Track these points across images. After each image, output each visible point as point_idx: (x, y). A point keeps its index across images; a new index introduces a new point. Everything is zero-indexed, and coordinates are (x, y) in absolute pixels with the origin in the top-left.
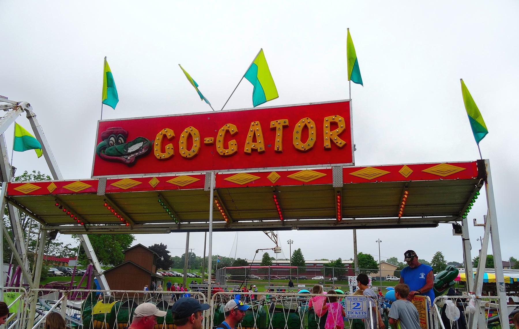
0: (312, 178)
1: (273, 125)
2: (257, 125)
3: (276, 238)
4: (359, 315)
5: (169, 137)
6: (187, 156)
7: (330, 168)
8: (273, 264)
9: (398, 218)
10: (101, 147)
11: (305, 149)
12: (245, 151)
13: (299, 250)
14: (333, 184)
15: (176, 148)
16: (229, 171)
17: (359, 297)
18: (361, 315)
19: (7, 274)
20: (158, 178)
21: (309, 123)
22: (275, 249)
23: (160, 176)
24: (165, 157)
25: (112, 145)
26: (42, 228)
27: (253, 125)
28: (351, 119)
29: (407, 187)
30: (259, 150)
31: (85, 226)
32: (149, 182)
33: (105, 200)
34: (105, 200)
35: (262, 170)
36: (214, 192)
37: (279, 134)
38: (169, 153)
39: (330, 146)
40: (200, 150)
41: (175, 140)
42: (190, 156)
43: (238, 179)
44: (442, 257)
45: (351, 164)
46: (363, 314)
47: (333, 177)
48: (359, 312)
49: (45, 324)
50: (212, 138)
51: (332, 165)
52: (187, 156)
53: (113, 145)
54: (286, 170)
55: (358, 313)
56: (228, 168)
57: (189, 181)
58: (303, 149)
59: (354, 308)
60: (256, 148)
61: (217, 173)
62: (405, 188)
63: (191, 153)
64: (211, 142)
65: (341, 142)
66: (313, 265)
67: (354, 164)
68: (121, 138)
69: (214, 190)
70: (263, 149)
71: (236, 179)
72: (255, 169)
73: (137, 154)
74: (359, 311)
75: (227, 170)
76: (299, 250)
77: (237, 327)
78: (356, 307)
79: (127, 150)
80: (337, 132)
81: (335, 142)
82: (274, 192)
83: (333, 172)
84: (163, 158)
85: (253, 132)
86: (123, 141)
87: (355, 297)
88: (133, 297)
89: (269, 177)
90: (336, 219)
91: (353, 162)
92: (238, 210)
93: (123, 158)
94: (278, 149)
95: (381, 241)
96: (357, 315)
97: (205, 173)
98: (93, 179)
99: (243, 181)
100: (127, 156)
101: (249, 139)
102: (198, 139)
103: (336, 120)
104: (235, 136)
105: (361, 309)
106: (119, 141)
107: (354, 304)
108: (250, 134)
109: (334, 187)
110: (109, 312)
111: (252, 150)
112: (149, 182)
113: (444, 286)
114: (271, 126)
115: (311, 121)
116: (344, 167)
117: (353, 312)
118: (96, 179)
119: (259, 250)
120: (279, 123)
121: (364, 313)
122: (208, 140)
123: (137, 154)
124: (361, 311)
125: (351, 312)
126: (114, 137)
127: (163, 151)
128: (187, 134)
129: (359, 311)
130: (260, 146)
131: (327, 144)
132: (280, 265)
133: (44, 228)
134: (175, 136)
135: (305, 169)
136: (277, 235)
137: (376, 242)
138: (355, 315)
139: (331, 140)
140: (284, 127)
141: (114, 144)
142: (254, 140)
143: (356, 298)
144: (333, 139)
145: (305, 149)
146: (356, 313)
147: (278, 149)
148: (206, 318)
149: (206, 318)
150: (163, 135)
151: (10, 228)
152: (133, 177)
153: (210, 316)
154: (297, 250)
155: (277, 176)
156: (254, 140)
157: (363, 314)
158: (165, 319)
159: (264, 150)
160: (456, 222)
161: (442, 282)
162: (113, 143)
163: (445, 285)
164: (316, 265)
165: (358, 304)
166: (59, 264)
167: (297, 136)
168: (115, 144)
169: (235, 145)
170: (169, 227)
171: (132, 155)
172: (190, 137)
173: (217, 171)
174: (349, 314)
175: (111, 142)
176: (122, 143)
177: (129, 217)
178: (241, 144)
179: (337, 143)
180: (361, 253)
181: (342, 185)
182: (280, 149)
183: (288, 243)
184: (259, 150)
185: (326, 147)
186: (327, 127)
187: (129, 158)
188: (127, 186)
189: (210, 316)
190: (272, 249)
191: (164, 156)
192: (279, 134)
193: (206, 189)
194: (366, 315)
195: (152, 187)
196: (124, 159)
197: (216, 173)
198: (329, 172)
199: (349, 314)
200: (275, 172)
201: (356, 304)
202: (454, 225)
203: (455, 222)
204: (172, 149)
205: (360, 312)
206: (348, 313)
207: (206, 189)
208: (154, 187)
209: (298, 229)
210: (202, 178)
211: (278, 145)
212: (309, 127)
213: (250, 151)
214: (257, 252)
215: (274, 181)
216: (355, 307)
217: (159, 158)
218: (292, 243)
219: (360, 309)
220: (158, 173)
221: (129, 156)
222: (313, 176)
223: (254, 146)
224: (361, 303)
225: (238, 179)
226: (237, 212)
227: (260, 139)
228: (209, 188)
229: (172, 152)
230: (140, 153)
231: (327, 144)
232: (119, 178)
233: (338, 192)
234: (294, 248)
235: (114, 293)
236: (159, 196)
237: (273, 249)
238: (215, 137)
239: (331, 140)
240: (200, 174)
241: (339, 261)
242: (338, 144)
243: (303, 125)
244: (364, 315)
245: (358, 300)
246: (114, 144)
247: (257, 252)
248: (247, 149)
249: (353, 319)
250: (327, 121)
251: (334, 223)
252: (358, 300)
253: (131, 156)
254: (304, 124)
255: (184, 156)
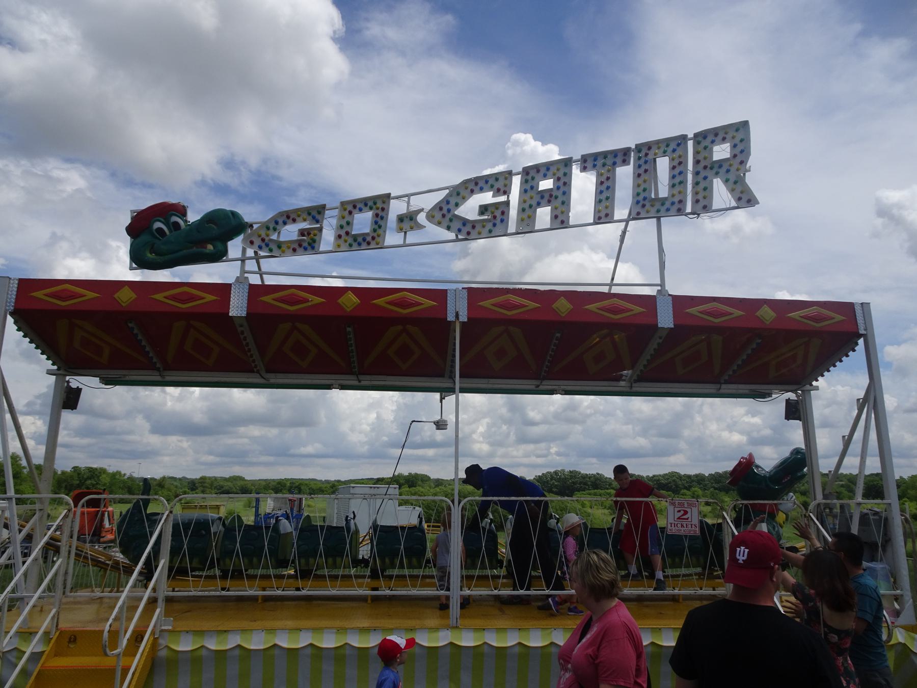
19: (408, 489)
46: (692, 527)
49: (120, 585)
55: (685, 526)
77: (25, 592)
78: (681, 516)
88: (380, 533)
105: (690, 520)
107: (679, 511)
117: (677, 524)
121: (693, 526)
125: (675, 524)
138: (680, 528)
146: (682, 526)
157: (692, 527)
158: (534, 546)
165: (686, 513)
166: (30, 477)
174: (671, 526)
180: (17, 330)
201: (682, 512)
219: (687, 519)
224: (689, 510)
241: (854, 350)
245: (686, 505)
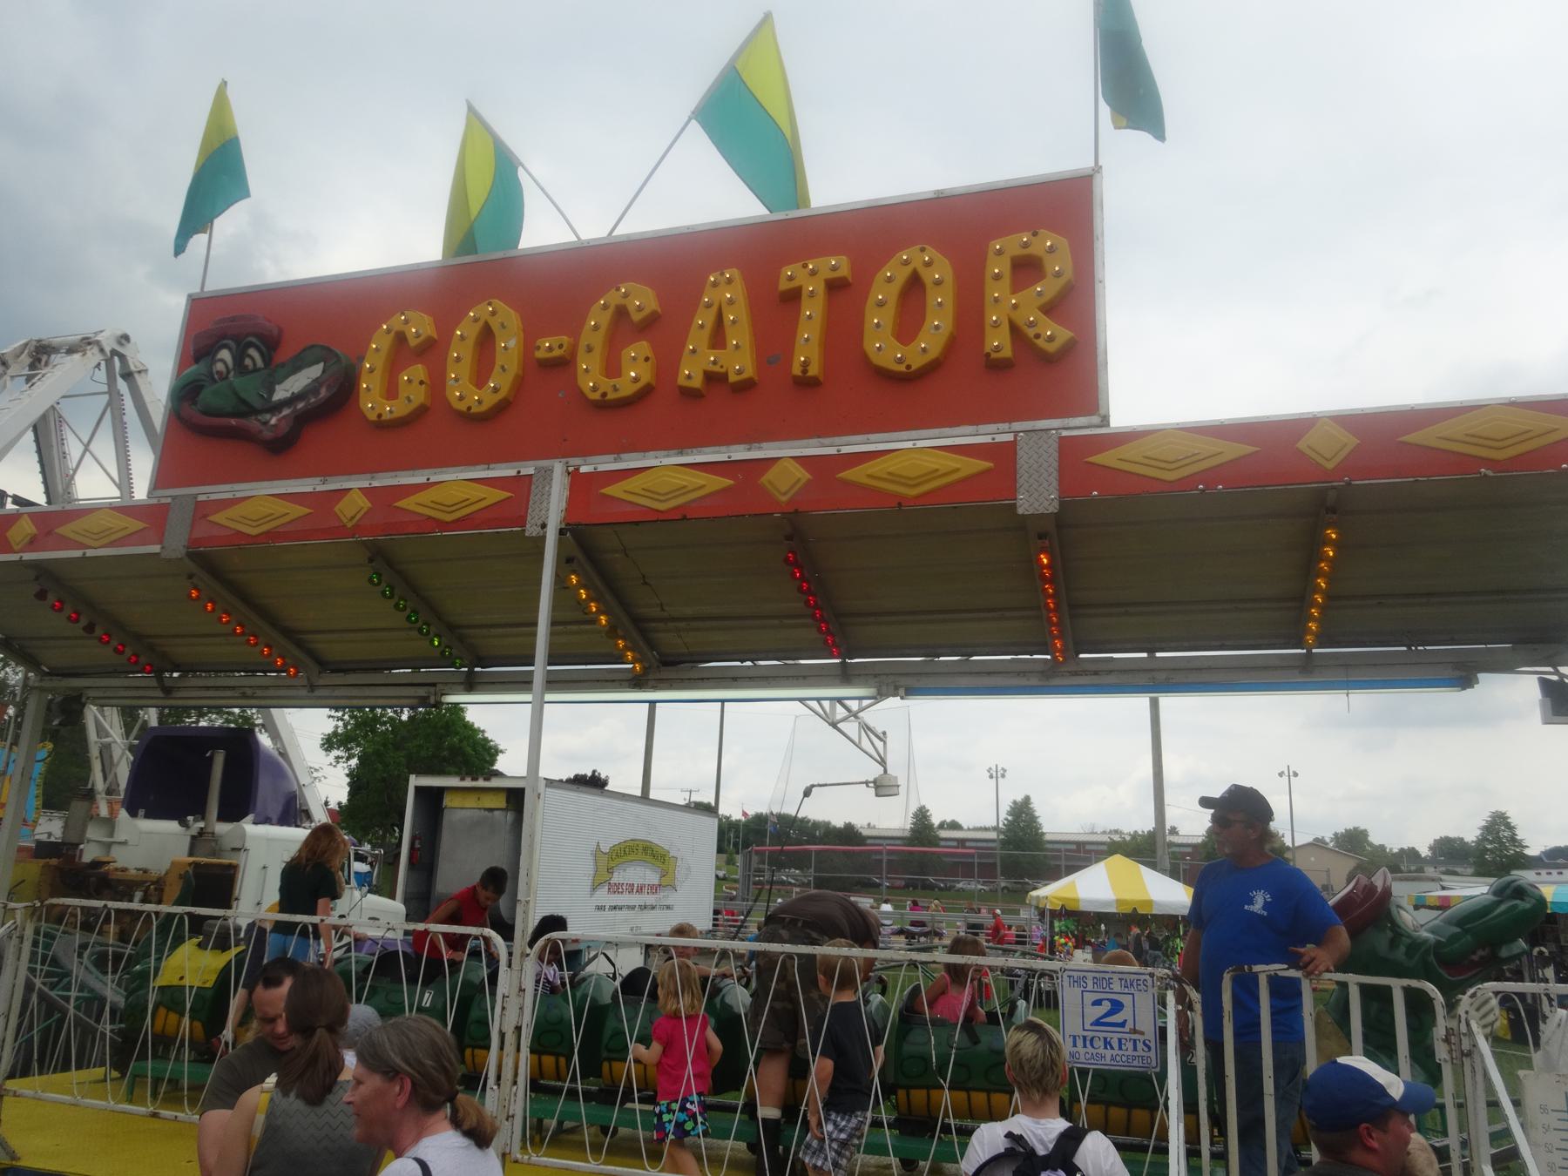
0: (935, 478)
1: (791, 278)
2: (730, 281)
3: (879, 744)
4: (1121, 1052)
5: (413, 342)
6: (469, 408)
7: (1009, 437)
8: (942, 843)
9: (1305, 651)
10: (188, 384)
11: (908, 367)
12: (681, 381)
13: (1027, 799)
14: (1019, 503)
15: (437, 383)
16: (621, 460)
17: (1121, 976)
18: (1126, 1053)
20: (367, 492)
21: (928, 264)
22: (875, 782)
23: (376, 484)
24: (396, 415)
25: (224, 377)
26: (31, 683)
27: (715, 284)
28: (1097, 245)
29: (1335, 513)
30: (733, 378)
31: (160, 678)
32: (336, 509)
33: (190, 576)
34: (190, 576)
35: (739, 453)
36: (561, 543)
37: (812, 311)
38: (409, 400)
39: (1007, 352)
40: (520, 384)
41: (431, 351)
42: (484, 408)
43: (649, 491)
44: (1510, 827)
45: (1095, 419)
47: (1021, 472)
48: (1120, 1040)
50: (565, 339)
51: (1017, 426)
52: (469, 408)
53: (227, 378)
54: (832, 451)
55: (1116, 1045)
56: (619, 449)
57: (473, 500)
58: (902, 368)
59: (1097, 1023)
60: (723, 370)
61: (577, 470)
62: (1327, 513)
63: (479, 399)
64: (557, 353)
65: (1051, 333)
66: (1074, 847)
67: (1105, 421)
68: (252, 352)
69: (562, 532)
70: (749, 373)
71: (643, 489)
72: (717, 448)
73: (300, 405)
74: (1120, 1036)
75: (613, 456)
76: (1027, 799)
79: (271, 392)
80: (1040, 294)
81: (1031, 332)
82: (787, 540)
83: (1020, 453)
84: (386, 417)
85: (714, 309)
86: (260, 363)
87: (1102, 975)
89: (770, 477)
90: (1049, 657)
91: (1102, 412)
92: (674, 619)
93: (252, 423)
94: (805, 371)
95: (1296, 775)
96: (1109, 1053)
97: (531, 471)
98: (154, 501)
99: (667, 497)
100: (268, 416)
101: (697, 339)
102: (512, 343)
103: (1035, 250)
104: (648, 327)
106: (248, 362)
107: (1097, 1003)
108: (704, 319)
109: (1020, 511)
110: (211, 981)
111: (710, 377)
112: (336, 509)
113: (1475, 958)
114: (784, 285)
115: (938, 257)
116: (1065, 433)
118: (163, 501)
119: (813, 786)
120: (813, 273)
121: (1140, 1046)
122: (548, 346)
123: (300, 405)
124: (1127, 1036)
125: (1085, 1038)
126: (230, 349)
127: (391, 392)
128: (478, 327)
129: (1120, 1036)
130: (739, 362)
131: (998, 342)
132: (968, 844)
133: (36, 685)
134: (435, 336)
135: (909, 445)
136: (884, 733)
137: (1281, 774)
138: (1102, 1051)
139: (1015, 329)
140: (835, 287)
141: (228, 372)
142: (718, 338)
143: (1107, 976)
144: (1020, 322)
145: (908, 367)
146: (1107, 1043)
147: (805, 371)
148: (502, 1036)
149: (502, 1036)
150: (393, 332)
151: (170, 711)
152: (283, 491)
153: (518, 1029)
154: (1019, 798)
155: (799, 476)
156: (718, 338)
159: (752, 375)
160: (1558, 671)
161: (1469, 937)
162: (224, 370)
163: (1481, 953)
164: (1084, 847)
165: (1117, 1006)
167: (878, 323)
168: (232, 373)
169: (647, 359)
170: (434, 685)
171: (286, 412)
172: (486, 338)
173: (575, 461)
175: (220, 367)
176: (256, 370)
177: (300, 644)
178: (667, 362)
179: (1038, 336)
181: (1056, 504)
182: (813, 371)
183: (991, 777)
184: (733, 378)
185: (994, 355)
186: (997, 277)
187: (273, 421)
188: (262, 521)
189: (518, 1029)
190: (867, 783)
191: (389, 409)
192: (812, 311)
193: (532, 530)
194: (1152, 1054)
195: (344, 526)
196: (258, 424)
197: (571, 469)
198: (1003, 455)
199: (1075, 1045)
200: (792, 461)
201: (1106, 1006)
202: (1546, 686)
203: (1550, 669)
204: (421, 383)
205: (1123, 1041)
206: (1070, 1041)
207: (532, 530)
208: (349, 525)
209: (902, 691)
210: (521, 485)
211: (807, 351)
212: (928, 281)
213: (697, 382)
214: (807, 793)
215: (785, 494)
216: (1101, 1018)
217: (372, 417)
218: (1003, 776)
219: (1123, 1024)
220: (368, 476)
221: (274, 415)
222: (940, 473)
223: (715, 363)
224: (1126, 1000)
225: (649, 491)
226: (671, 625)
227: (739, 336)
228: (544, 526)
229: (418, 396)
230: (313, 400)
231: (998, 342)
232: (239, 495)
233: (1041, 536)
234: (1011, 794)
235: (112, 911)
236: (371, 560)
237: (871, 785)
238: (575, 333)
239: (1015, 329)
240: (513, 473)
242: (1040, 342)
243: (903, 275)
244: (1144, 1054)
245: (1116, 987)
246: (228, 372)
247: (807, 793)
248: (690, 373)
249: (1094, 1070)
250: (1000, 253)
251: (1042, 672)
252: (1116, 987)
253: (281, 415)
254: (908, 270)
255: (462, 407)
